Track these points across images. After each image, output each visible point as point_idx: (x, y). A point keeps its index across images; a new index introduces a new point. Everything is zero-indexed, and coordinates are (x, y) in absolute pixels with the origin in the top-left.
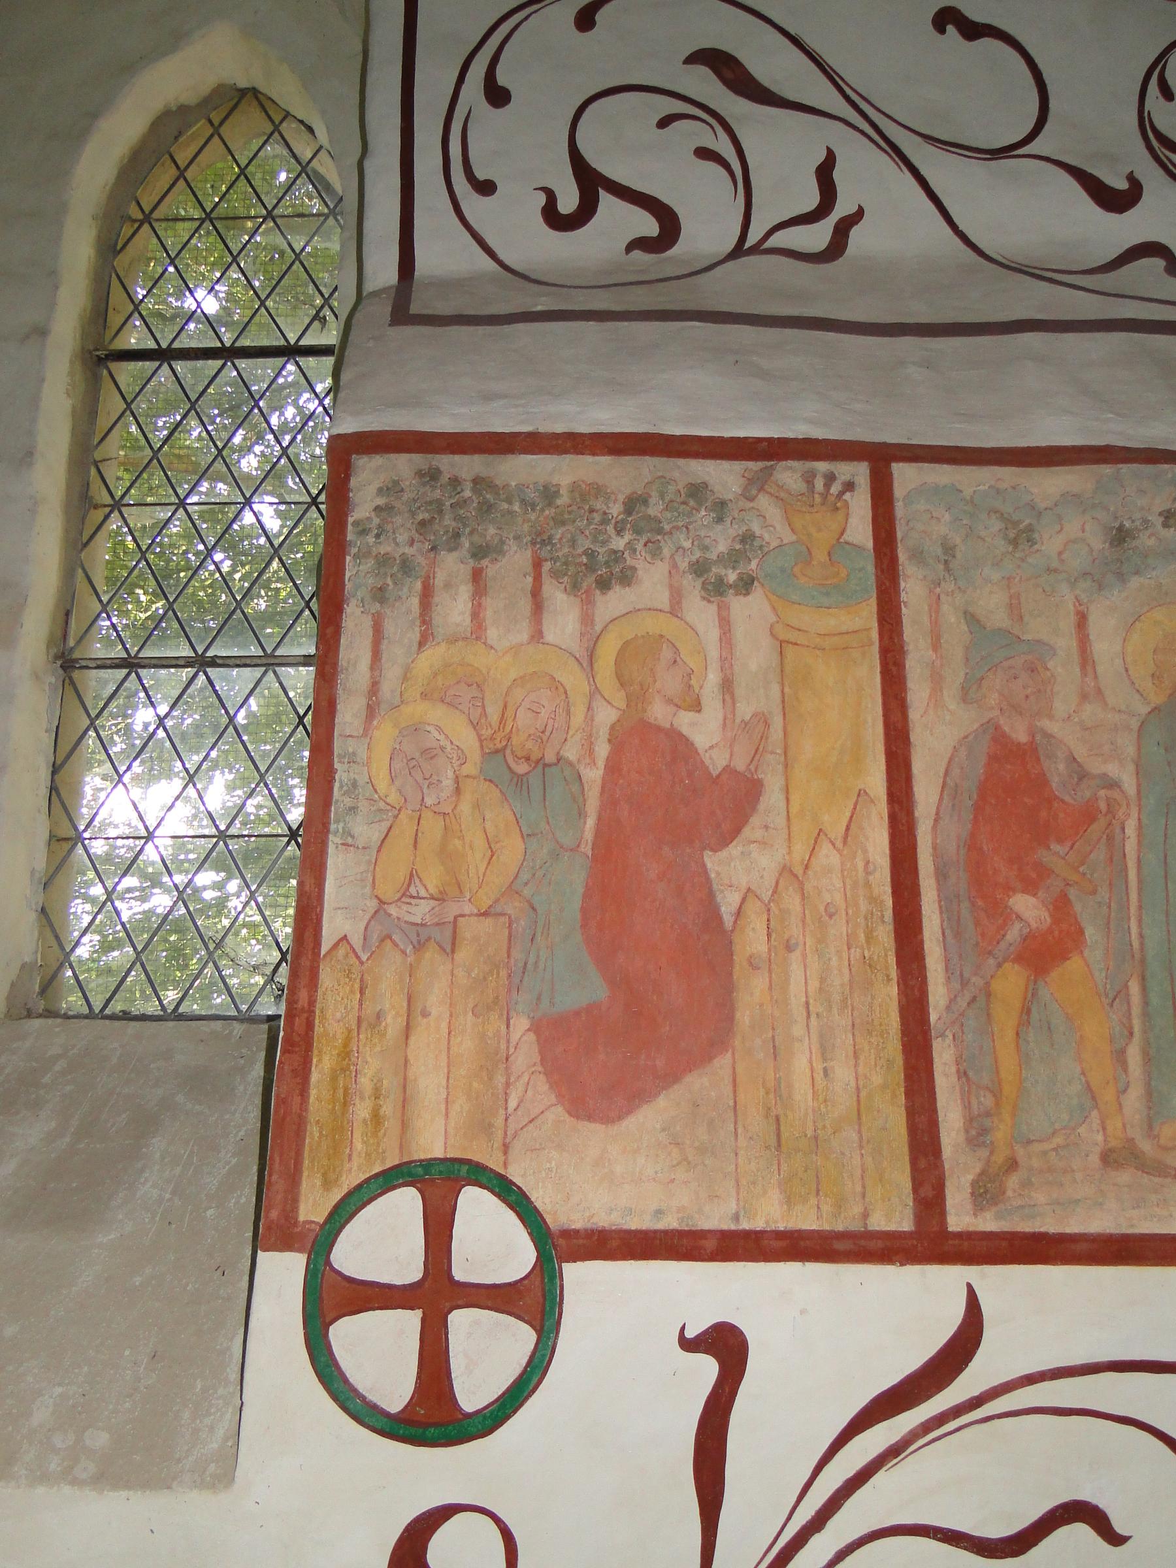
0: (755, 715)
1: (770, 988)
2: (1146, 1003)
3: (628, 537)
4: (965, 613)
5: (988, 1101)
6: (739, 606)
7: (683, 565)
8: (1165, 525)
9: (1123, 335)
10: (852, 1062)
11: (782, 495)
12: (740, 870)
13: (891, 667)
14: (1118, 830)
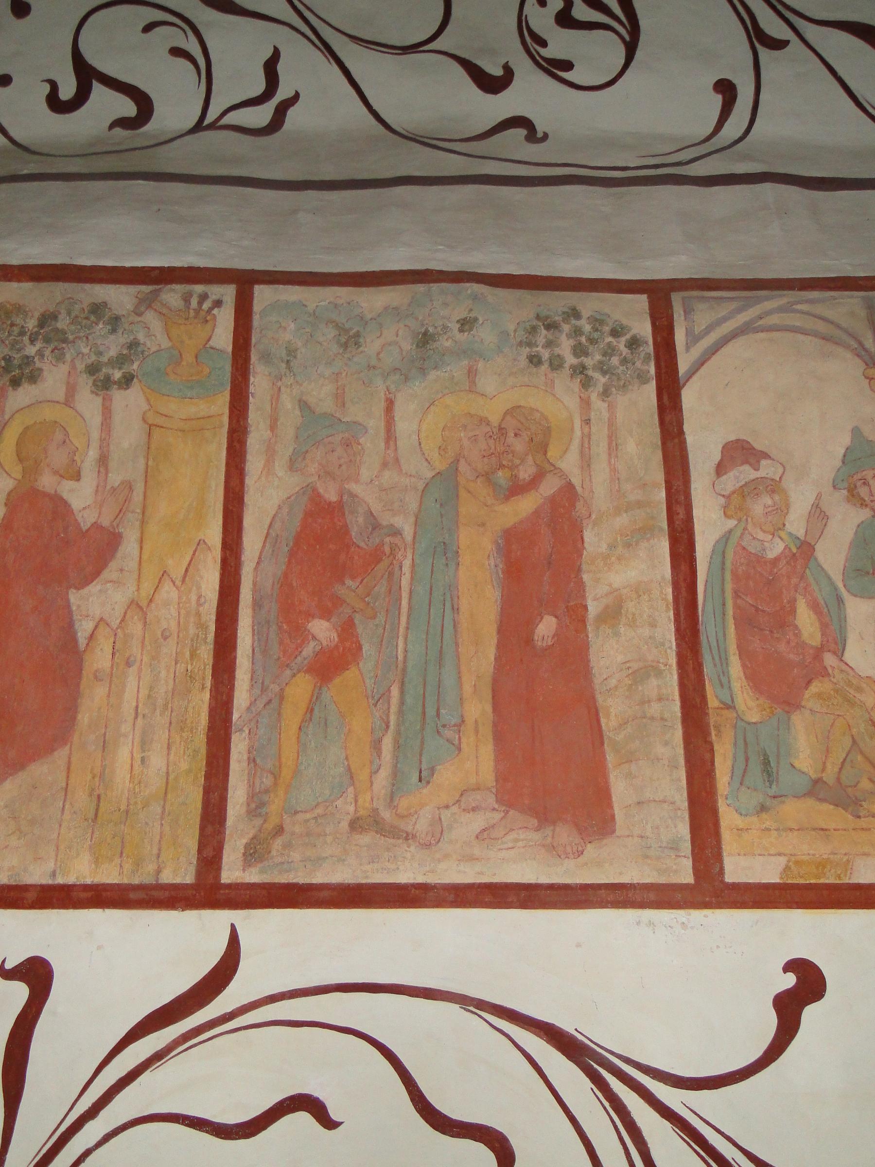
0: (122, 483)
1: (108, 696)
2: (402, 702)
3: (39, 345)
4: (300, 401)
5: (268, 781)
6: (119, 397)
7: (80, 366)
8: (461, 331)
9: (476, 187)
10: (165, 752)
11: (164, 311)
12: (95, 604)
13: (235, 444)
14: (397, 569)
